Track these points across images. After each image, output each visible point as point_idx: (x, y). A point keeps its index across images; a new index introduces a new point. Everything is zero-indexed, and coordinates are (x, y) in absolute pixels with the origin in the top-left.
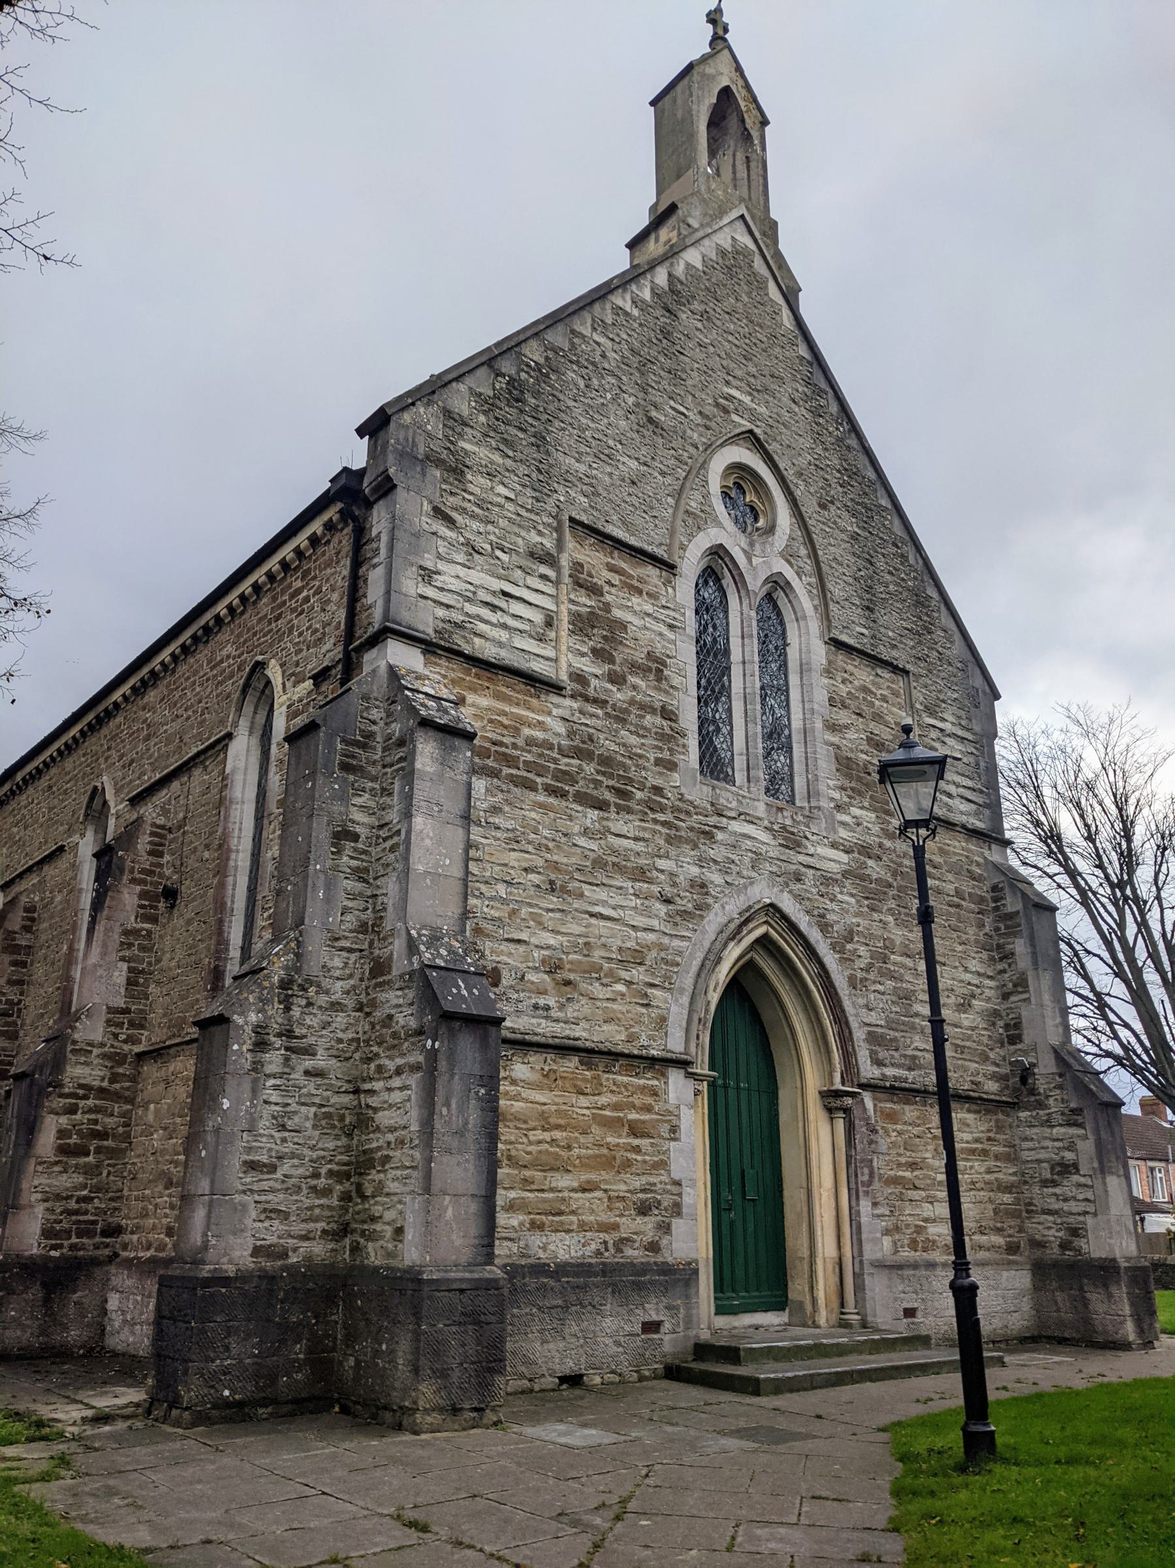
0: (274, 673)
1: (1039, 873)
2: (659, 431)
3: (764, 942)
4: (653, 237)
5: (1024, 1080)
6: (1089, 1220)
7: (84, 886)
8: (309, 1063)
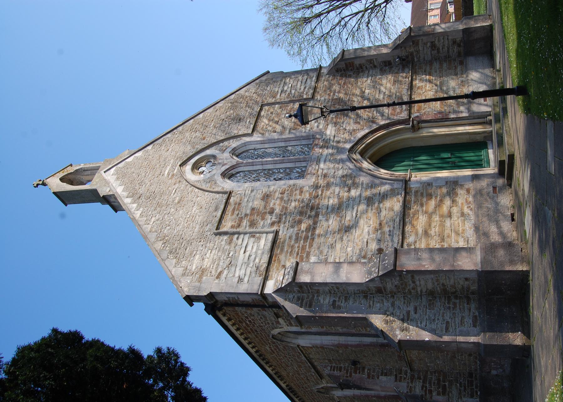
0: (276, 332)
1: (315, 22)
2: (182, 199)
3: (362, 154)
4: (113, 204)
5: (404, 60)
6: (450, 38)
7: (352, 394)
8: (412, 313)
